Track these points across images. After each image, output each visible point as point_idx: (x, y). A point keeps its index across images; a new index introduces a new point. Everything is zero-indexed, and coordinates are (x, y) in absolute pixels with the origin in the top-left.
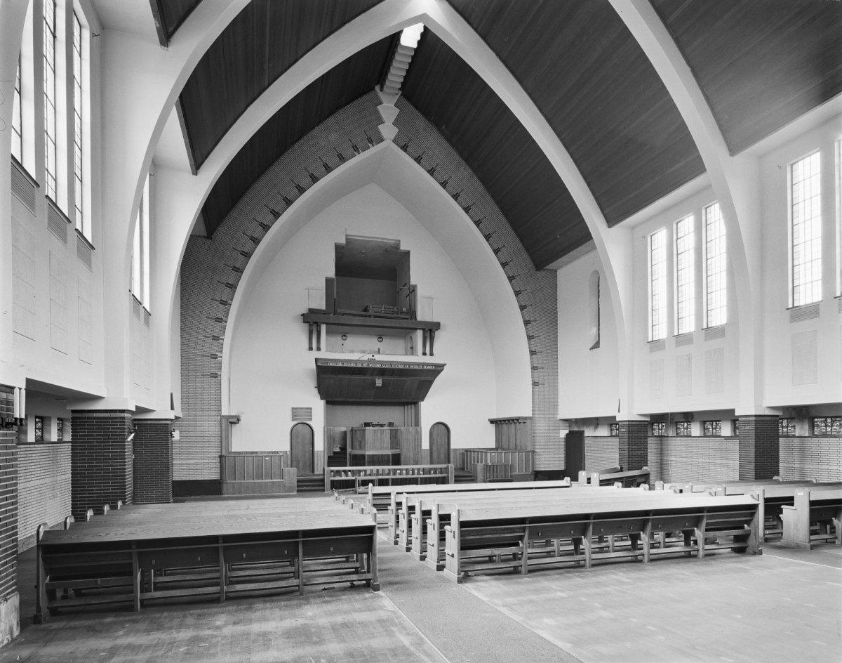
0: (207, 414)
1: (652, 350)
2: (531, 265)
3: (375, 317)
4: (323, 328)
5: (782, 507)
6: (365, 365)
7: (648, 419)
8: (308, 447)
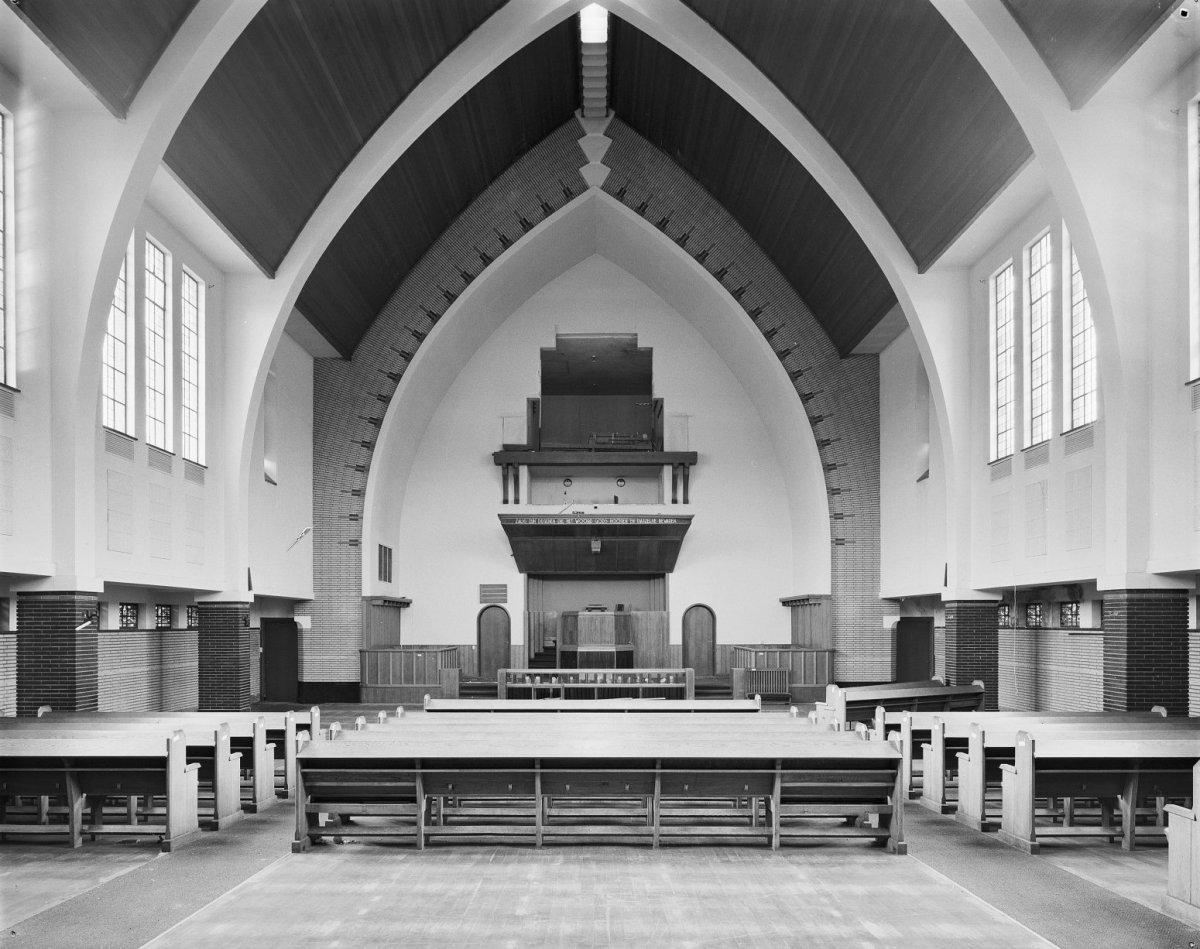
0: (346, 594)
1: (995, 476)
2: (829, 348)
3: (597, 450)
4: (524, 471)
5: (1002, 766)
6: (569, 522)
7: (999, 598)
8: (502, 641)
